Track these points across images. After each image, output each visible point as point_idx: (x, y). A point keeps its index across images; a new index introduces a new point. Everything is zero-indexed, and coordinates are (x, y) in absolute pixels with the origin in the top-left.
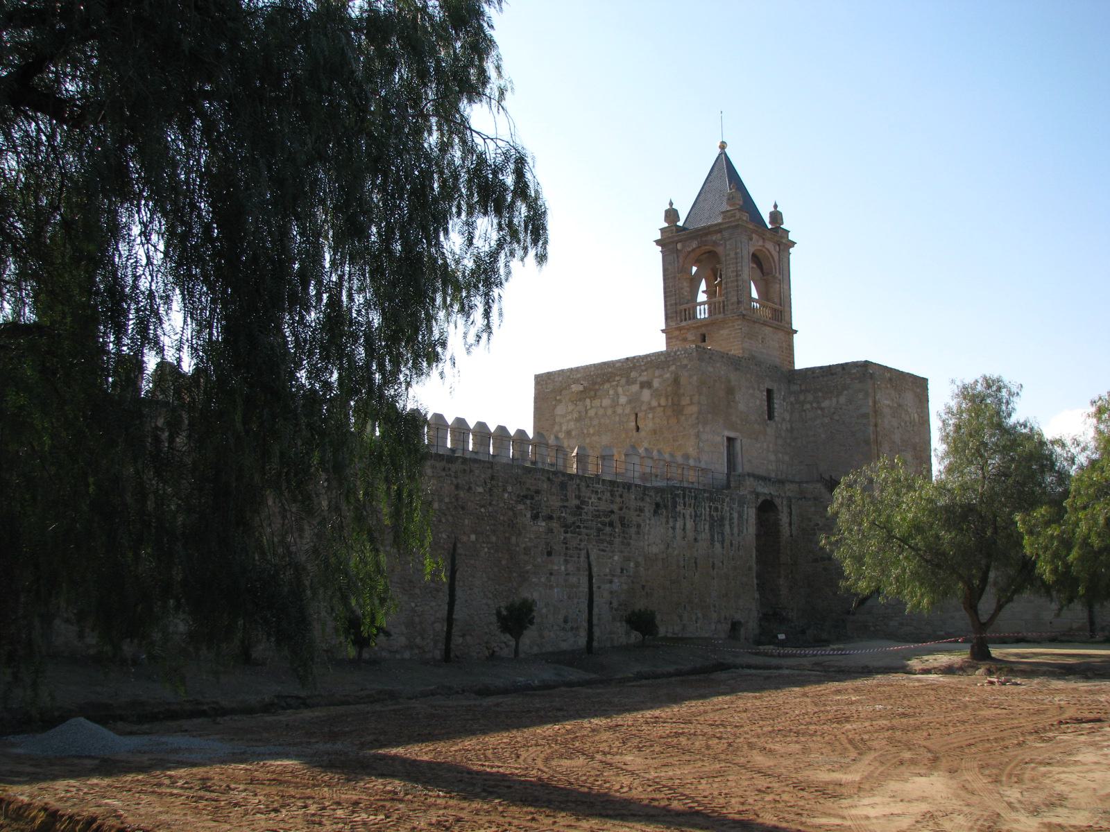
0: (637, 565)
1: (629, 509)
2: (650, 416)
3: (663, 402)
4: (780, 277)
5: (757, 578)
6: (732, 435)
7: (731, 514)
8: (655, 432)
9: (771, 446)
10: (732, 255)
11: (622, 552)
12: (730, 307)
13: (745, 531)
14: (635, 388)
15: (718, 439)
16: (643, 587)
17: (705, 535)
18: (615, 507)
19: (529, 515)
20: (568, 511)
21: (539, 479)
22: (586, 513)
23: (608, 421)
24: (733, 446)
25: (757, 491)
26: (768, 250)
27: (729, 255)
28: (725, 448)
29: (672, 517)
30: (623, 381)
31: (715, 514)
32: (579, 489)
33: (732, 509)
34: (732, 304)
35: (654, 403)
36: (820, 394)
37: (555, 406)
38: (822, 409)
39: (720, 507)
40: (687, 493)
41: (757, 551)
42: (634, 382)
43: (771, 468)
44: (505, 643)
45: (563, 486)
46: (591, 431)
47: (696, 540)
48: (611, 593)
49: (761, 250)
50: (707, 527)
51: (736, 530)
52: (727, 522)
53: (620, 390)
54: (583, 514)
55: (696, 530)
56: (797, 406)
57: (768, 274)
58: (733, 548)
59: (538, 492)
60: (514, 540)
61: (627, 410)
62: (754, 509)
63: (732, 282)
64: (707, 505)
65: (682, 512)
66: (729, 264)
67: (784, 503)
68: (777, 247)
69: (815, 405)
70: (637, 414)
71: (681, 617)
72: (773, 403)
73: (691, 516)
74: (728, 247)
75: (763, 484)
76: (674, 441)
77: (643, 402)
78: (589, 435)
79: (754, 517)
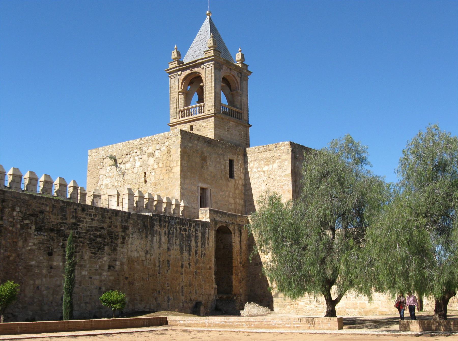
0: (122, 264)
1: (116, 227)
2: (153, 174)
3: (161, 165)
4: (241, 93)
5: (215, 275)
6: (204, 186)
7: (196, 234)
9: (231, 194)
11: (109, 255)
13: (206, 244)
15: (195, 188)
16: (127, 278)
17: (176, 247)
18: (105, 226)
19: (33, 227)
20: (67, 226)
21: (43, 204)
22: (81, 228)
24: (205, 192)
25: (216, 220)
26: (234, 76)
27: (207, 77)
28: (199, 194)
29: (150, 234)
31: (184, 233)
32: (76, 213)
33: (196, 230)
34: (209, 107)
35: (156, 166)
36: (262, 162)
39: (188, 229)
40: (162, 218)
41: (215, 257)
43: (231, 207)
44: (12, 314)
45: (62, 209)
47: (168, 249)
48: (101, 281)
49: (229, 76)
50: (178, 241)
51: (199, 244)
52: (193, 239)
54: (79, 229)
55: (169, 242)
57: (234, 90)
58: (197, 255)
59: (41, 212)
60: (20, 244)
62: (214, 232)
63: (209, 93)
64: (178, 227)
65: (158, 230)
66: (208, 83)
67: (236, 228)
68: (240, 75)
69: (259, 169)
70: (145, 173)
71: (156, 299)
72: (233, 168)
73: (165, 233)
74: (207, 72)
75: (221, 216)
76: (166, 189)
79: (214, 236)
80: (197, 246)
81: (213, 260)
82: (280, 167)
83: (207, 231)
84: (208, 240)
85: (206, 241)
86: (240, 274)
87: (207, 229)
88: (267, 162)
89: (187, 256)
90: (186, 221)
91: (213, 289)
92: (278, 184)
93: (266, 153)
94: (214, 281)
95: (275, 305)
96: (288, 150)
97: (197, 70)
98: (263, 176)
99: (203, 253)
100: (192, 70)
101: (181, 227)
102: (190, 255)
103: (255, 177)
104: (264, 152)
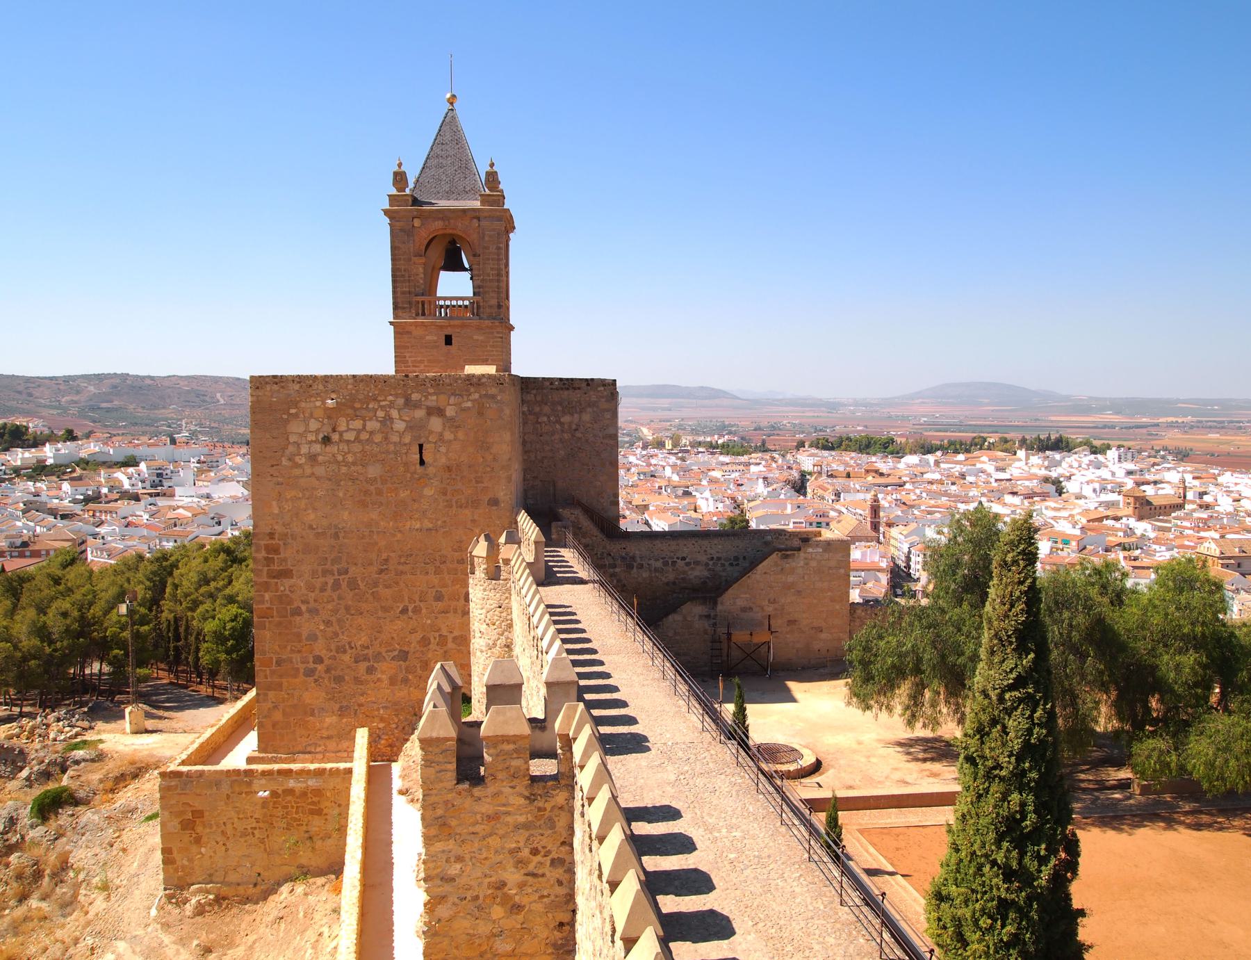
2: (443, 449)
8: (449, 469)
10: (493, 249)
12: (488, 310)
14: (420, 413)
23: (376, 449)
27: (487, 248)
30: (401, 401)
34: (491, 307)
37: (287, 422)
38: (562, 424)
42: (417, 405)
46: (350, 458)
53: (395, 414)
56: (531, 417)
61: (407, 439)
63: (491, 281)
70: (421, 446)
76: (477, 482)
77: (431, 432)
78: (347, 464)
93: (566, 393)
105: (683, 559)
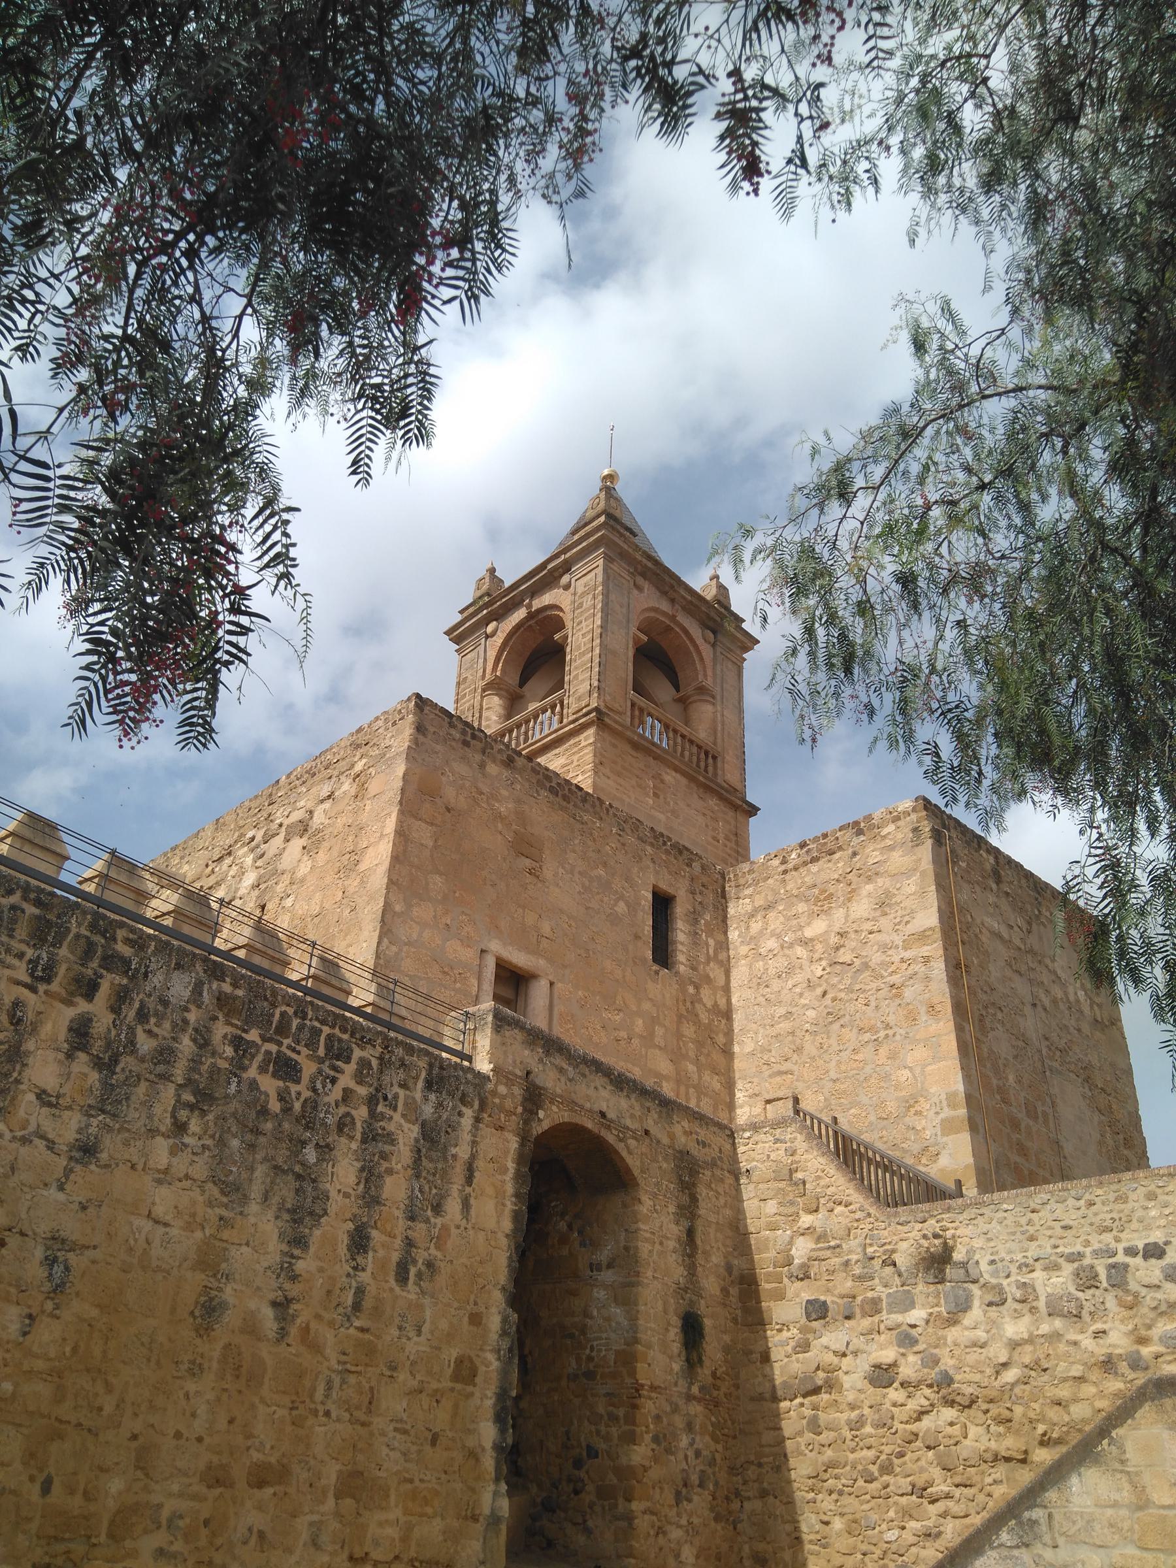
5: (499, 1419)
6: (520, 959)
9: (659, 1031)
13: (453, 1206)
36: (801, 907)
38: (805, 942)
39: (309, 1068)
64: (221, 1030)
80: (371, 1200)
81: (494, 1322)
82: (883, 904)
83: (467, 1122)
84: (469, 1180)
85: (455, 1189)
86: (684, 1441)
87: (468, 1113)
88: (822, 901)
89: (275, 1247)
90: (301, 1014)
91: (479, 1527)
92: (879, 983)
93: (814, 868)
94: (489, 1462)
95: (650, 896)
96: (915, 830)
97: (546, 599)
98: (806, 963)
99: (421, 1256)
100: (529, 606)
101: (253, 1035)
102: (299, 1242)
103: (772, 971)
104: (805, 864)
105: (1154, 1252)
